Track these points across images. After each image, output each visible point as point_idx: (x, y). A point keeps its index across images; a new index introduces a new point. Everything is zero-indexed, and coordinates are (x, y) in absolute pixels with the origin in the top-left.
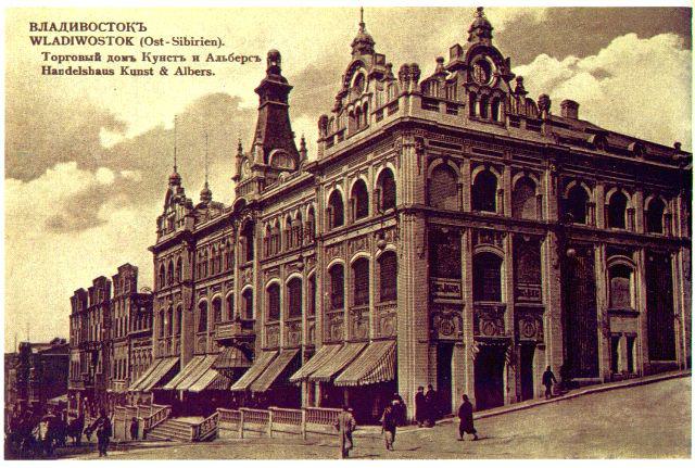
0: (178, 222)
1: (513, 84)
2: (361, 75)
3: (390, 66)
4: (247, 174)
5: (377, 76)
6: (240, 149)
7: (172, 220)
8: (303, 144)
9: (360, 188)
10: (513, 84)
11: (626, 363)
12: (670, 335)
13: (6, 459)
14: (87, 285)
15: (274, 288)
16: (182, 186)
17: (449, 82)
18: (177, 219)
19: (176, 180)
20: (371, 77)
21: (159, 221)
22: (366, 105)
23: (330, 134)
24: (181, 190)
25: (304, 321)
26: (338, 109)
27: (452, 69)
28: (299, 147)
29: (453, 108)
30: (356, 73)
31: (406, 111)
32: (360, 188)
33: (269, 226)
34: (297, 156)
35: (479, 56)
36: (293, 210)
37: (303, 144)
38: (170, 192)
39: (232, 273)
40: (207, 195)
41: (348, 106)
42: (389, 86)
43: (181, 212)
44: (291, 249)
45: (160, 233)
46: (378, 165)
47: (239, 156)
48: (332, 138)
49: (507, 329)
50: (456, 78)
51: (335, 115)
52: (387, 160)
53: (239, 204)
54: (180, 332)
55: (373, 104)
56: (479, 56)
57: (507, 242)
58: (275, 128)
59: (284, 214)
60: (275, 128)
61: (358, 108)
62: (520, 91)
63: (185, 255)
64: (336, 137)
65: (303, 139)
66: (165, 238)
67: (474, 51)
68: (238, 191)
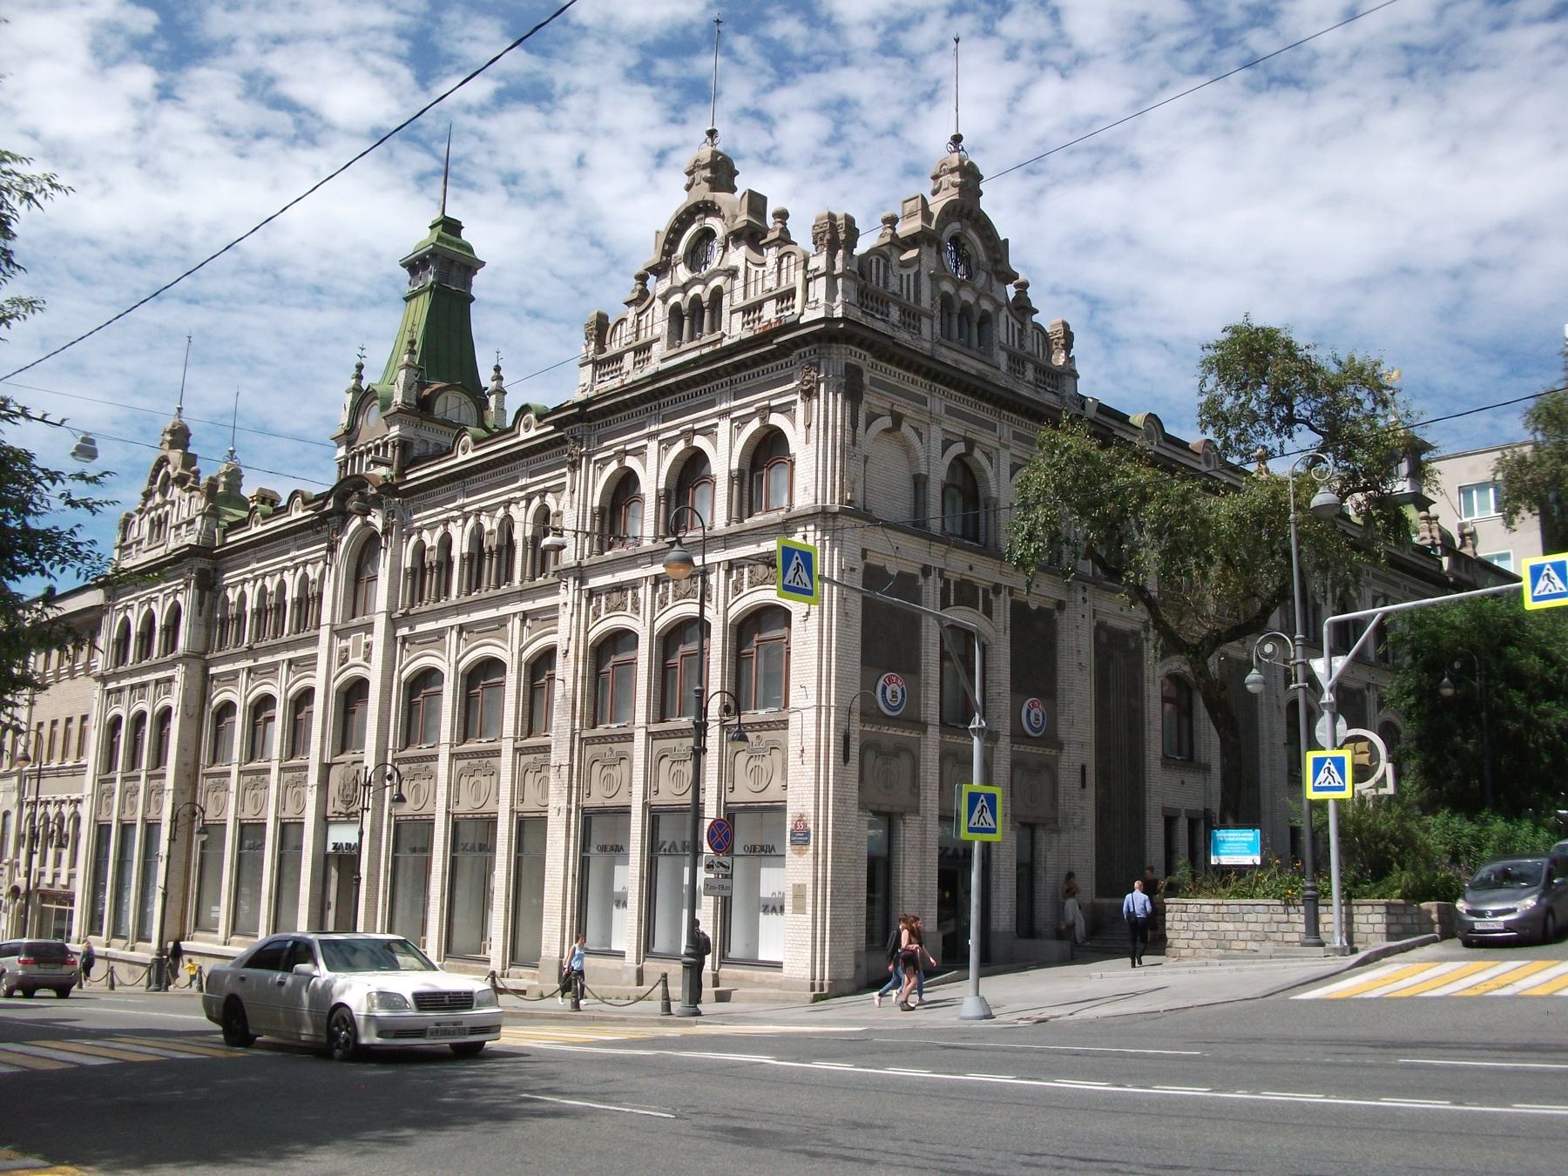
0: (178, 527)
2: (708, 234)
3: (782, 215)
6: (359, 377)
7: (159, 524)
9: (150, 619)
10: (1011, 291)
12: (519, 1020)
13: (1164, 809)
15: (428, 677)
16: (190, 450)
17: (905, 265)
18: (173, 521)
20: (736, 237)
22: (717, 294)
23: (613, 348)
24: (189, 460)
25: (640, 736)
26: (641, 298)
27: (912, 241)
30: (694, 228)
32: (150, 619)
33: (305, 576)
35: (955, 227)
36: (272, 575)
38: (163, 462)
39: (314, 641)
41: (715, 274)
42: (780, 259)
43: (186, 506)
46: (671, 442)
47: (356, 390)
48: (619, 357)
50: (917, 259)
51: (631, 313)
53: (350, 489)
55: (738, 293)
56: (955, 227)
57: (1002, 606)
59: (529, 499)
61: (696, 300)
62: (1023, 307)
63: (186, 600)
64: (629, 358)
65: (497, 369)
67: (950, 211)
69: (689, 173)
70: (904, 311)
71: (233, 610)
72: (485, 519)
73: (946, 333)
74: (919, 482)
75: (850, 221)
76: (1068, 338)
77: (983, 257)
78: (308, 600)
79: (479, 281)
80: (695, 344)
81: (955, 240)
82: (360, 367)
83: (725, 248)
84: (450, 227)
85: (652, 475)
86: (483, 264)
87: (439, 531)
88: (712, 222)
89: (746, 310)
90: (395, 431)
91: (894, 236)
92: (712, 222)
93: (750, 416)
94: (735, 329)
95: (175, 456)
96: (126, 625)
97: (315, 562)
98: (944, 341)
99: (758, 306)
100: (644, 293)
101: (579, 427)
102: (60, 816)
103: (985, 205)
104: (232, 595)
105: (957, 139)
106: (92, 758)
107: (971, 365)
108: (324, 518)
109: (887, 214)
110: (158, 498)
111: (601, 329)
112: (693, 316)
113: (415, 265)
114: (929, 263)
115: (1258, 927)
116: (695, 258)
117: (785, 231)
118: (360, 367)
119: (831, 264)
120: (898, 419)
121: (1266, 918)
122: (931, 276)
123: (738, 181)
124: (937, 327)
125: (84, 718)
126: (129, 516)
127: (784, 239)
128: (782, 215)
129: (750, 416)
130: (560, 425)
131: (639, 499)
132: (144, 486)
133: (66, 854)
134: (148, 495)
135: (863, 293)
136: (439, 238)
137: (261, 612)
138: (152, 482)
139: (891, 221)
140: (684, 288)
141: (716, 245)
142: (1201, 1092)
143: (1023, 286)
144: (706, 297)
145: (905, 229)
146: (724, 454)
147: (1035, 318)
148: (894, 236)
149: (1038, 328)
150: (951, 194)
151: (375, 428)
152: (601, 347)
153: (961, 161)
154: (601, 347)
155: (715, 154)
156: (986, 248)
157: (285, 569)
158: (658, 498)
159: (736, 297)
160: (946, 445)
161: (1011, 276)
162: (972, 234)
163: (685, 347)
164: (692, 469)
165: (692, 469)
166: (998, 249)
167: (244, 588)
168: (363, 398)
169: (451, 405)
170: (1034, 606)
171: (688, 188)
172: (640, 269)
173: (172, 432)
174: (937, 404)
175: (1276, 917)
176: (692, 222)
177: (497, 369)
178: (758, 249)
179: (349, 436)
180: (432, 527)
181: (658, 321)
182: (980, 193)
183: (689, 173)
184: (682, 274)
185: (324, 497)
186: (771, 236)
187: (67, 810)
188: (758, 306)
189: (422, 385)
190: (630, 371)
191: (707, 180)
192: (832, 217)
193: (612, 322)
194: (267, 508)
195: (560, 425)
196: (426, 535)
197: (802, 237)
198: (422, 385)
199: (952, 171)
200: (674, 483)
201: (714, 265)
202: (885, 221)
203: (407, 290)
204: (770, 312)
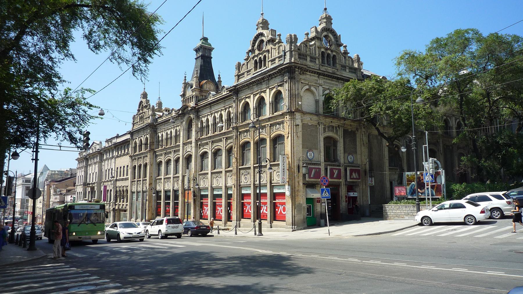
1: (342, 49)
2: (262, 41)
3: (279, 35)
4: (189, 93)
5: (272, 41)
6: (185, 80)
7: (141, 118)
8: (219, 78)
11: (218, 212)
14: (332, 21)
19: (145, 95)
21: (134, 118)
24: (148, 101)
27: (313, 39)
28: (217, 80)
29: (313, 59)
31: (291, 59)
33: (176, 130)
34: (218, 86)
37: (219, 78)
38: (141, 102)
40: (160, 104)
42: (279, 47)
44: (216, 133)
45: (239, 76)
48: (243, 74)
49: (28, 221)
50: (315, 44)
52: (246, 98)
53: (184, 108)
54: (145, 176)
57: (341, 132)
58: (205, 70)
60: (205, 70)
62: (346, 53)
64: (246, 74)
65: (219, 75)
66: (136, 127)
67: (324, 30)
68: (183, 101)
69: (257, 25)
70: (311, 58)
71: (160, 138)
72: (216, 114)
73: (323, 62)
74: (317, 102)
75: (295, 36)
76: (358, 59)
77: (333, 40)
78: (177, 136)
79: (213, 54)
80: (261, 70)
81: (326, 37)
82: (185, 77)
83: (266, 45)
84: (205, 39)
85: (252, 102)
86: (214, 49)
87: (219, 113)
88: (263, 38)
89: (272, 61)
90: (194, 94)
91: (308, 38)
92: (263, 38)
93: (258, 93)
94: (270, 66)
95: (144, 100)
96: (136, 143)
97: (178, 126)
98: (323, 65)
99: (274, 60)
100: (249, 57)
101: (236, 91)
102: (123, 191)
103: (334, 27)
104: (160, 135)
105: (326, 9)
106: (129, 176)
107: (330, 70)
108: (179, 115)
109: (306, 32)
110: (141, 112)
111: (239, 66)
112: (259, 63)
113: (197, 50)
114: (318, 44)
115: (406, 212)
116: (260, 48)
117: (280, 39)
118: (185, 77)
119: (291, 48)
120: (310, 86)
121: (404, 209)
122: (318, 47)
123: (269, 26)
124: (320, 60)
125: (127, 166)
126: (135, 116)
127: (280, 42)
128: (279, 35)
129: (258, 93)
130: (230, 91)
131: (265, 104)
132: (138, 108)
133: (125, 200)
134: (139, 110)
135: (300, 54)
136: (202, 43)
137: (167, 139)
138: (139, 108)
139: (307, 34)
140: (257, 56)
141: (265, 43)
142: (433, 268)
143: (345, 47)
144: (262, 58)
145: (311, 35)
146: (268, 97)
147: (349, 55)
148: (308, 38)
149: (350, 57)
150: (323, 25)
151: (189, 93)
152: (239, 71)
153: (326, 15)
154: (239, 71)
155: (263, 20)
156: (334, 38)
157: (208, 115)
158: (254, 109)
159: (269, 57)
160: (324, 91)
161: (341, 45)
162: (330, 35)
163: (258, 70)
164: (261, 101)
165: (261, 101)
166: (337, 38)
167: (162, 134)
168: (186, 85)
169: (208, 86)
170: (350, 130)
171: (257, 29)
172: (247, 51)
173: (143, 95)
174: (321, 81)
175: (411, 209)
176: (258, 38)
177: (219, 75)
178: (275, 45)
179: (183, 95)
180: (217, 112)
181: (251, 65)
182: (332, 24)
183: (257, 25)
184: (257, 52)
185: (179, 110)
186: (277, 41)
187: (121, 189)
188: (274, 60)
189: (200, 82)
190: (246, 78)
191: (261, 27)
192: (291, 35)
193: (242, 64)
194: (167, 113)
195: (230, 91)
196: (203, 119)
197: (284, 39)
198: (200, 82)
199: (324, 19)
200: (257, 105)
201: (264, 49)
202: (306, 34)
203: (196, 57)
204: (277, 63)
